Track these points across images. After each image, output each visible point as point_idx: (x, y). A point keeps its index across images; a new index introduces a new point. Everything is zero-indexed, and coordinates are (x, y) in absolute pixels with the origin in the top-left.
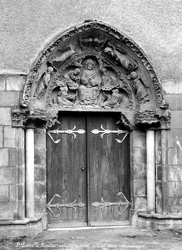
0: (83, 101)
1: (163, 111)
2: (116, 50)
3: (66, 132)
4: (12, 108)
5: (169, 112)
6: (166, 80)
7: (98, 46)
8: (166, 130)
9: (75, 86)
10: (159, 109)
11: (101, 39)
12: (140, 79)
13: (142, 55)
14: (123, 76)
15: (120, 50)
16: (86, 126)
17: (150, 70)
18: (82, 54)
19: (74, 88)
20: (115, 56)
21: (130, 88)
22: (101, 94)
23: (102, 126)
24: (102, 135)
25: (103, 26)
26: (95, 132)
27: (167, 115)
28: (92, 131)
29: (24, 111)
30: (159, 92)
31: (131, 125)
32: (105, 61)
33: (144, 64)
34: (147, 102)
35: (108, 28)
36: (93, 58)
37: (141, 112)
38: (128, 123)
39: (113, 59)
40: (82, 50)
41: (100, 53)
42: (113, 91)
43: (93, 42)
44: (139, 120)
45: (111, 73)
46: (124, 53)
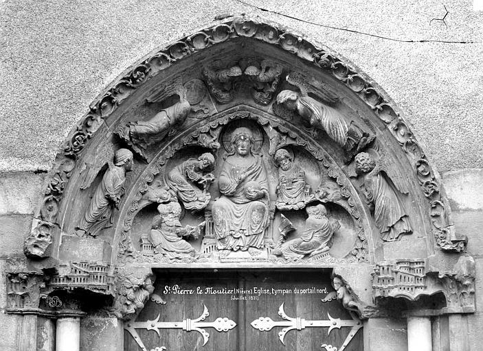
0: (222, 240)
1: (452, 258)
2: (310, 95)
3: (180, 325)
4: (8, 261)
5: (469, 263)
6: (459, 170)
7: (261, 91)
8: (464, 315)
9: (199, 199)
10: (441, 256)
11: (267, 69)
12: (383, 174)
13: (381, 100)
14: (336, 168)
15: (321, 95)
16: (238, 311)
17: (408, 144)
18: (217, 113)
19: (198, 206)
20: (309, 112)
21: (357, 199)
22: (277, 221)
23: (281, 308)
24: (282, 334)
25: (264, 28)
26: (263, 324)
27: (465, 272)
28: (253, 324)
29: (39, 268)
30: (437, 204)
31: (362, 303)
32: (283, 129)
33: (390, 127)
34: (405, 237)
35: (278, 32)
36: (254, 125)
37: (384, 264)
38: (355, 298)
39: (304, 121)
40: (218, 103)
41: (270, 109)
42: (309, 210)
43: (244, 77)
44: (381, 289)
45: (305, 162)
46: (333, 103)
